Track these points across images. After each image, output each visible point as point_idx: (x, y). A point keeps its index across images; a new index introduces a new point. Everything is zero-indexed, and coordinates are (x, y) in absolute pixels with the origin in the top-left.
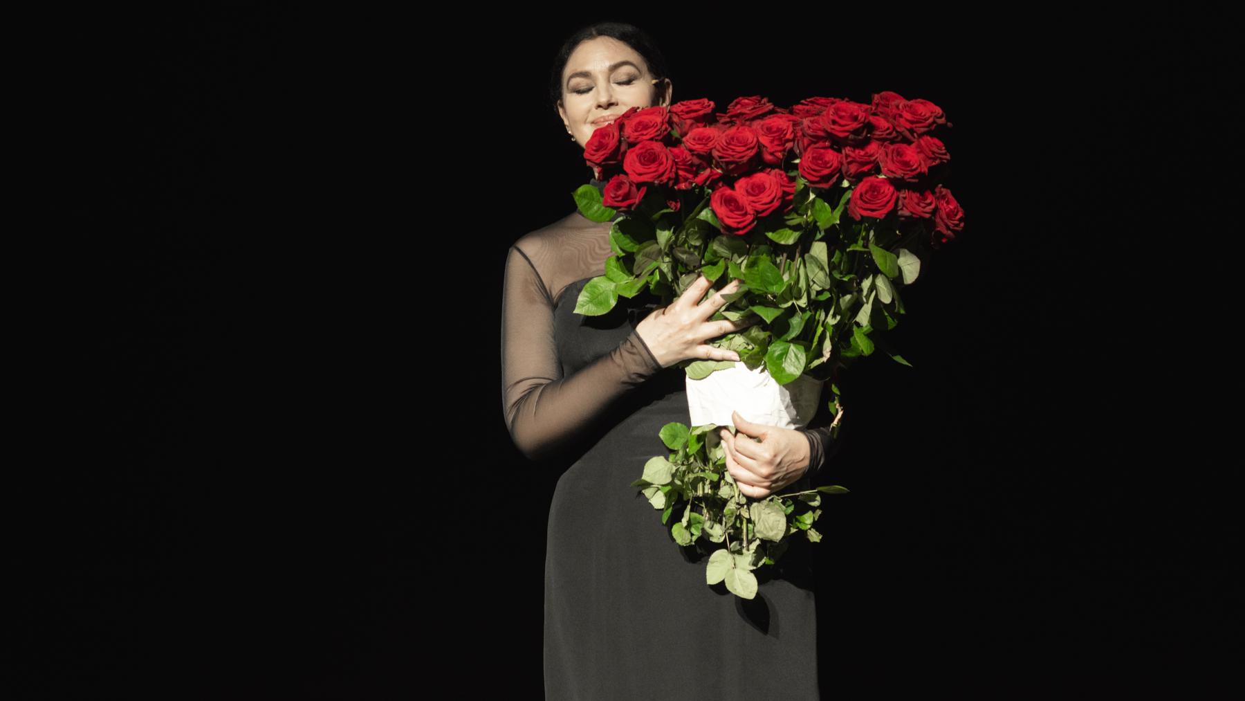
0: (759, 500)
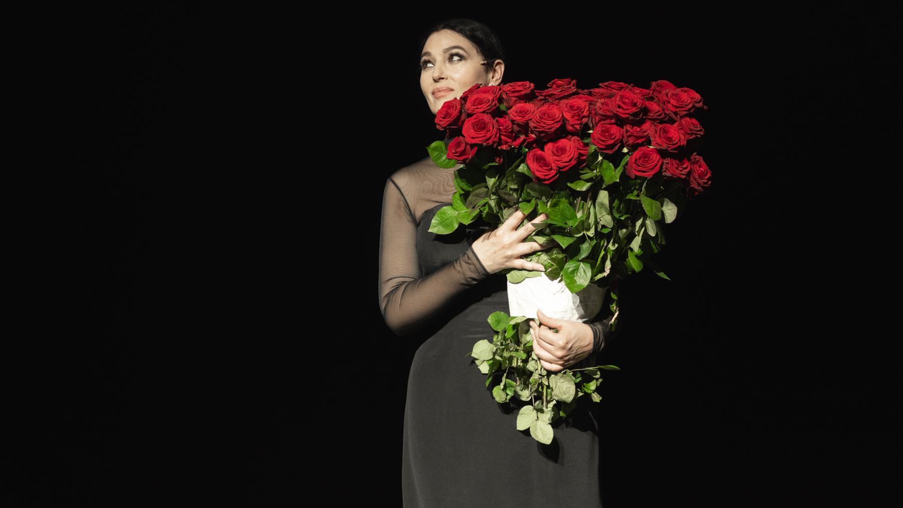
0: (556, 373)
